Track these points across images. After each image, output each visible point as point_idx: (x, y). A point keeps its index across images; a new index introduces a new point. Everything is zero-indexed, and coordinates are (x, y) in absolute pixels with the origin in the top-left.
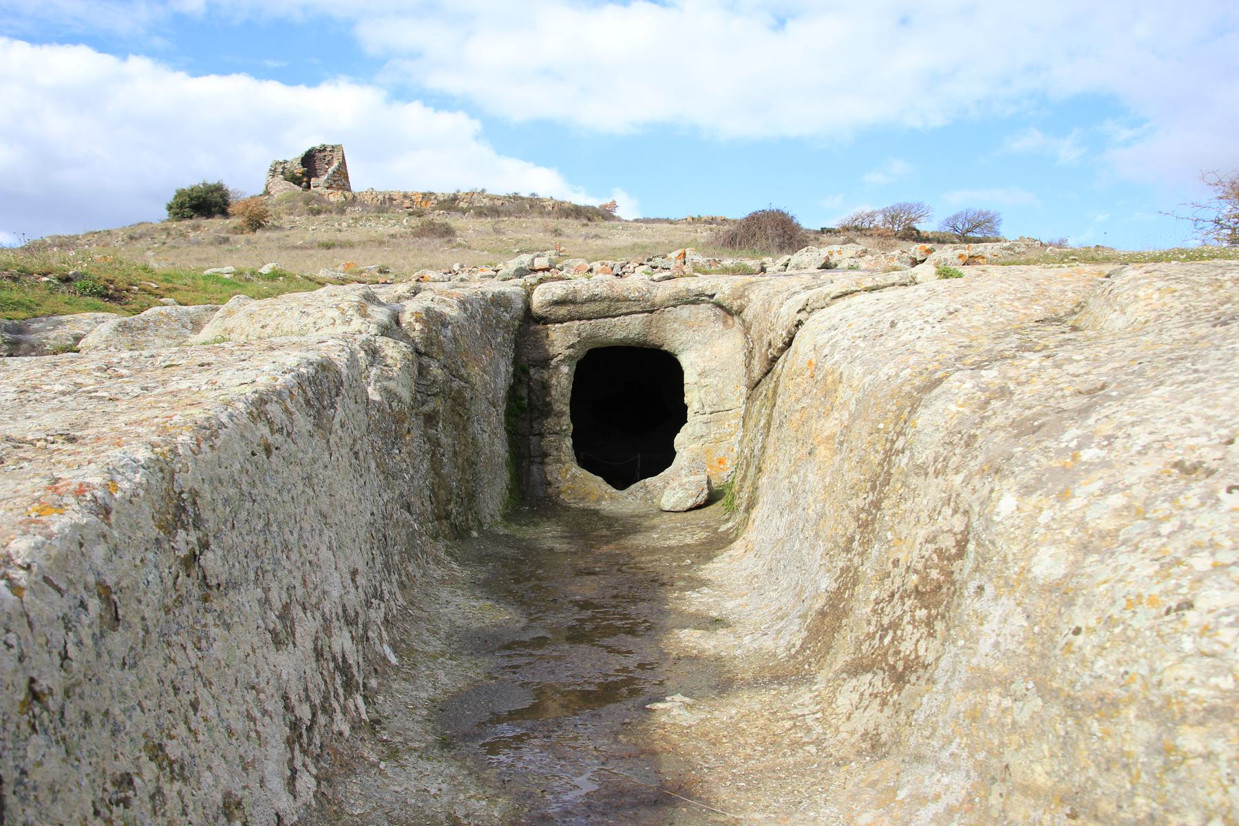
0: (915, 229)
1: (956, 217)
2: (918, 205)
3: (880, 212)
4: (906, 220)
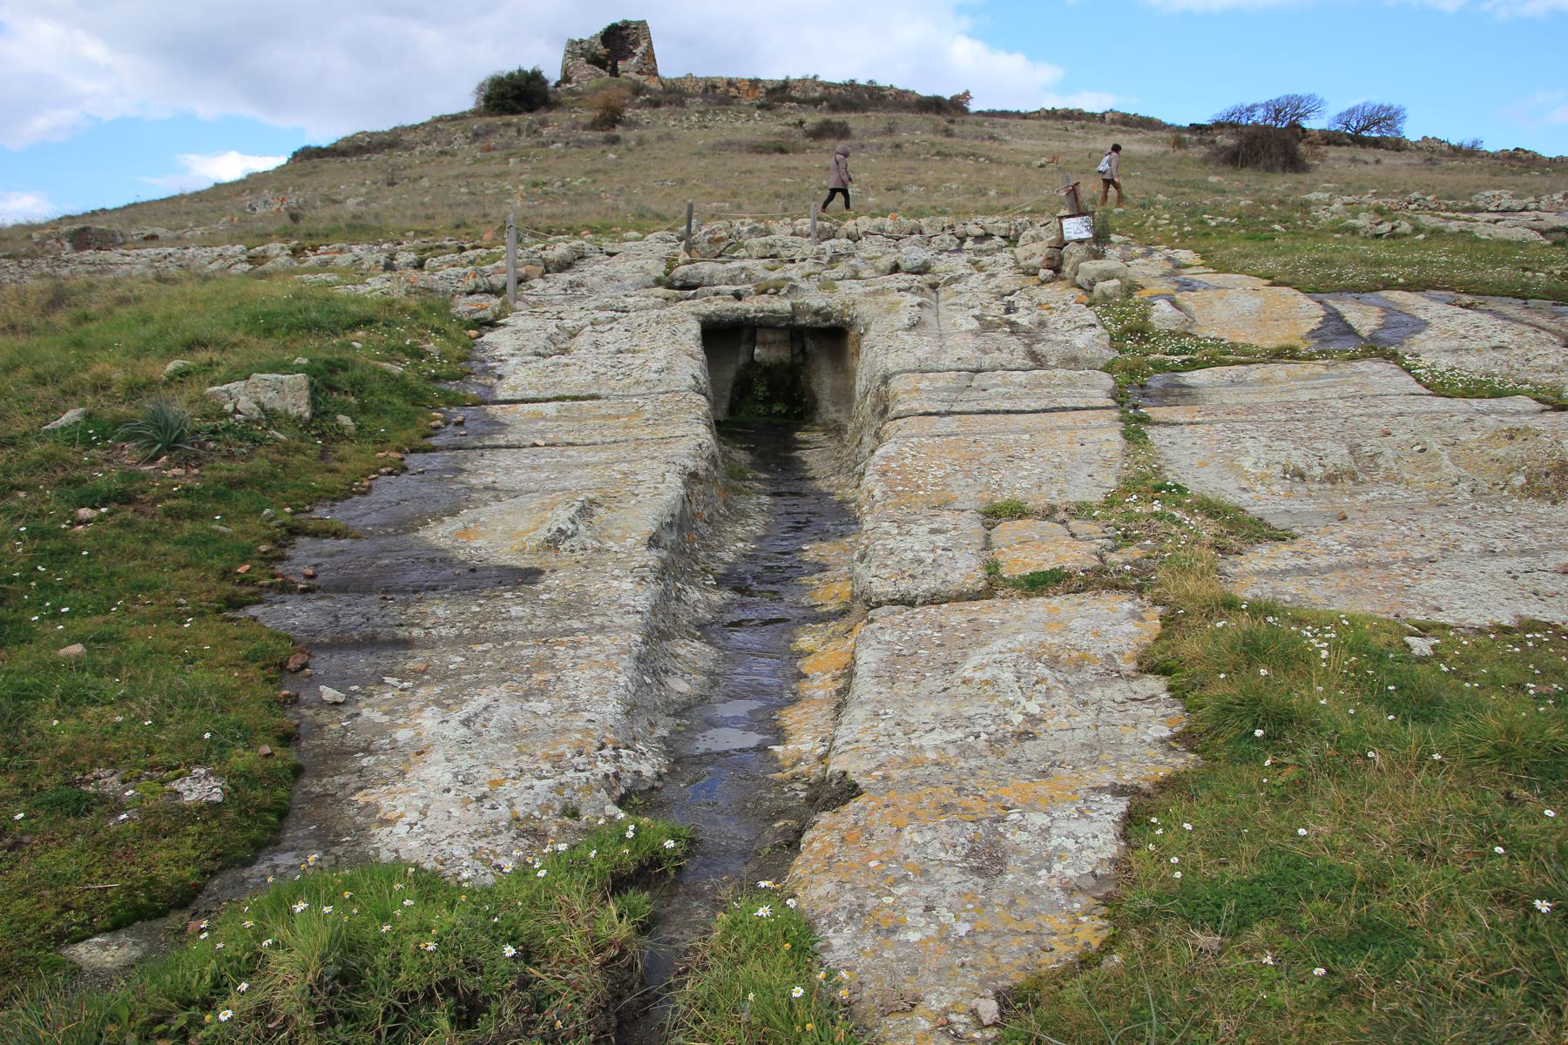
0: (1299, 126)
1: (1351, 112)
2: (1309, 98)
3: (1263, 106)
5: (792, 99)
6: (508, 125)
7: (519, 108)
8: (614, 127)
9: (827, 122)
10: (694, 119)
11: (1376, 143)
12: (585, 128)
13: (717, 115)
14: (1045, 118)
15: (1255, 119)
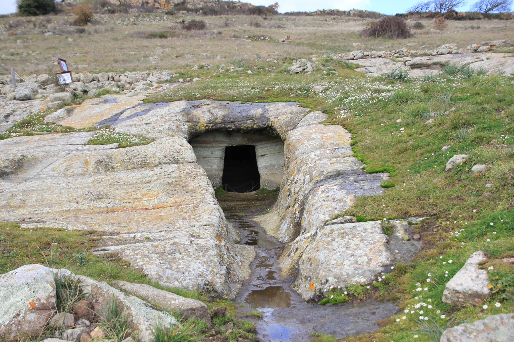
0: (454, 11)
3: (433, 2)
4: (449, 6)
5: (185, 9)
6: (30, 22)
7: (38, 12)
8: (86, 24)
9: (194, 21)
10: (132, 20)
11: (498, 17)
12: (71, 24)
13: (144, 17)
14: (319, 15)
15: (430, 9)
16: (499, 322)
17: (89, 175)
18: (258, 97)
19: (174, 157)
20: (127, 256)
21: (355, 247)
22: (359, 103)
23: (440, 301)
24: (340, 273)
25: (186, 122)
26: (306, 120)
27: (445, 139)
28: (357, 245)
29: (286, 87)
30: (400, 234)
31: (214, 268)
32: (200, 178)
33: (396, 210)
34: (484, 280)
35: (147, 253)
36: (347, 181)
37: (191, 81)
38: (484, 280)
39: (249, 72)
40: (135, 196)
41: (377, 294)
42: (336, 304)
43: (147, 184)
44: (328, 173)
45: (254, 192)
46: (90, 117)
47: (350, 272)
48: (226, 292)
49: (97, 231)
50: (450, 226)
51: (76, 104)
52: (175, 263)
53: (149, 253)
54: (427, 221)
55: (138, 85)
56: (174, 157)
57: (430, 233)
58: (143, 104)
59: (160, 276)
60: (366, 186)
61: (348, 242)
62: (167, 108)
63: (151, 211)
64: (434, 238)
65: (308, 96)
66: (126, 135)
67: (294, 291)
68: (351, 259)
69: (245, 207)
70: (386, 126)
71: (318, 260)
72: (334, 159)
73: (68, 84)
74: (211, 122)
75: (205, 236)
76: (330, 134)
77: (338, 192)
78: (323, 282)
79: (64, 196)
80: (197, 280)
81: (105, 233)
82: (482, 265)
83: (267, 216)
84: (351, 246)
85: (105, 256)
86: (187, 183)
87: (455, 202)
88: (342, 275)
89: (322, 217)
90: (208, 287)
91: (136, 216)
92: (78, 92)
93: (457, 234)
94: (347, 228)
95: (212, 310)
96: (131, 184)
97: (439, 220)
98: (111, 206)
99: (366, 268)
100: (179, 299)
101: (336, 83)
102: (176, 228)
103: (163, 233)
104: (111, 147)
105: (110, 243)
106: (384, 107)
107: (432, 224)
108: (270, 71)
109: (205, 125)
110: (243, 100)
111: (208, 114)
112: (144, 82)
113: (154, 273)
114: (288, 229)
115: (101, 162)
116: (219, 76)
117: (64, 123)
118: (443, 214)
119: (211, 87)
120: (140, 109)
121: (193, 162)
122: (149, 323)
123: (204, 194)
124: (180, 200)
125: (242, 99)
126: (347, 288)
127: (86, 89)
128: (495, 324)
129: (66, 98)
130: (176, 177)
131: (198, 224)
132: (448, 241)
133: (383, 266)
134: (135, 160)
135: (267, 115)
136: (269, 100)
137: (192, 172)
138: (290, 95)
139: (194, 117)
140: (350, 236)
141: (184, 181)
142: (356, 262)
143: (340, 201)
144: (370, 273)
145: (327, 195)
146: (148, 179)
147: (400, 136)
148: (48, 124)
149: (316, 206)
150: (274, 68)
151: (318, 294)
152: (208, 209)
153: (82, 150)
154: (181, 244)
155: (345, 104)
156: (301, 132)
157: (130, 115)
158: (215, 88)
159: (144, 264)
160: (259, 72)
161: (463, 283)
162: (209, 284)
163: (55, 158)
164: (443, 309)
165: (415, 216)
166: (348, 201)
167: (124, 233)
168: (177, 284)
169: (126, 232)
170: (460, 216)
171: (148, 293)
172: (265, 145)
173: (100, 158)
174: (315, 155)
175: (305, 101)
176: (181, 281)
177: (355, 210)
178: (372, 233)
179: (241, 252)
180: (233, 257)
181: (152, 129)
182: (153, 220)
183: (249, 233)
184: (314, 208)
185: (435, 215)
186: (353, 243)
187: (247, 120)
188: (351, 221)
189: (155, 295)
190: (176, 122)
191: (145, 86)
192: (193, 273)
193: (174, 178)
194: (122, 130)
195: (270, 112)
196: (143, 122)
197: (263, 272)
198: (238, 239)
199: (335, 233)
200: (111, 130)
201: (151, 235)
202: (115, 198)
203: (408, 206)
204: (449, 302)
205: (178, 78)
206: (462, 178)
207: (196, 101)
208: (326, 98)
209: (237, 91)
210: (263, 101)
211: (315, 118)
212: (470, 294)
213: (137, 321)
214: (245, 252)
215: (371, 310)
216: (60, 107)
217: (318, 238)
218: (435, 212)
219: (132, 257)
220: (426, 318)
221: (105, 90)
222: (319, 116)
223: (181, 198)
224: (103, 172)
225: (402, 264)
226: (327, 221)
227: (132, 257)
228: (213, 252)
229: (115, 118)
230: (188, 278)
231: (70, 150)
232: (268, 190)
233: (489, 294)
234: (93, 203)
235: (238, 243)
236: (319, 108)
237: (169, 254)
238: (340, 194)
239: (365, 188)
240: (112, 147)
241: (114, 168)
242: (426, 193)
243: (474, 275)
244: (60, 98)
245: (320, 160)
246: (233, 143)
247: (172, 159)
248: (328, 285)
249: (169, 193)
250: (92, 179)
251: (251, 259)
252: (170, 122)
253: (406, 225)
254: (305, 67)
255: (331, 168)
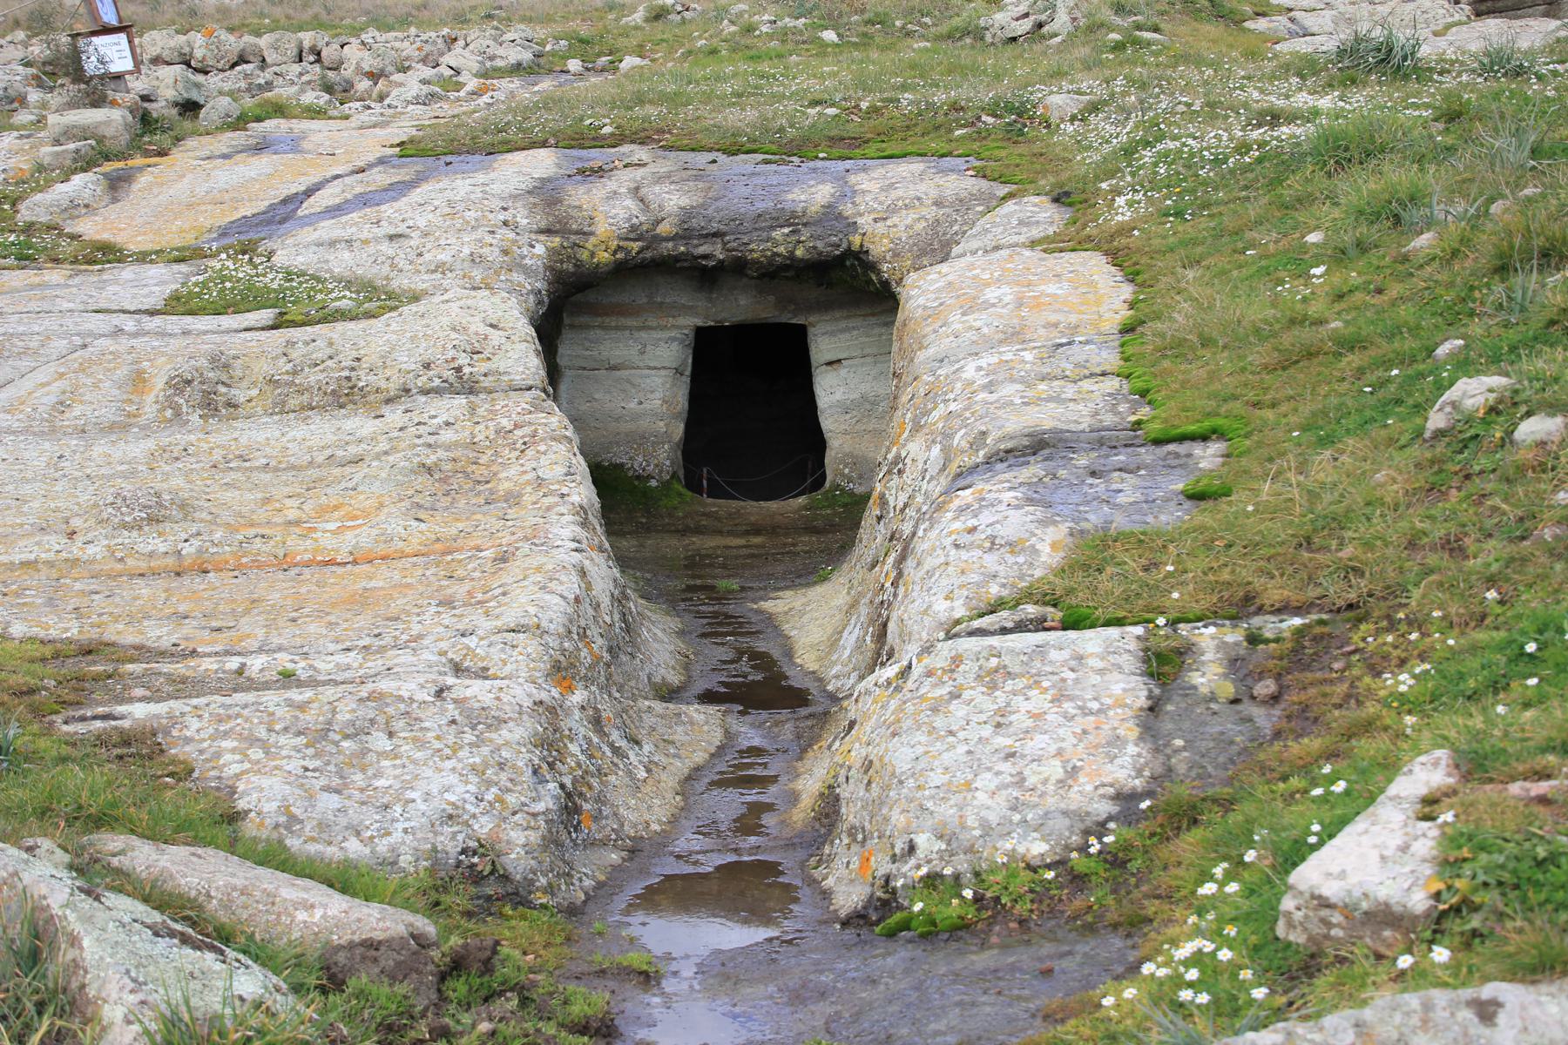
16: (1415, 1020)
17: (142, 428)
18: (831, 139)
19: (459, 369)
20: (188, 740)
21: (1029, 723)
22: (1188, 167)
23: (1270, 936)
24: (956, 820)
25: (541, 232)
26: (987, 231)
27: (1454, 317)
28: (1037, 716)
29: (940, 97)
30: (1208, 676)
31: (509, 790)
32: (542, 448)
33: (1213, 587)
34: (1424, 861)
35: (262, 733)
36: (1062, 473)
37: (612, 67)
38: (1424, 861)
39: (830, 36)
40: (292, 514)
41: (1078, 903)
42: (932, 934)
43: (348, 470)
44: (1003, 439)
45: (801, 500)
46: (190, 206)
47: (993, 818)
48: (543, 881)
49: (113, 644)
50: (1395, 653)
51: (147, 154)
52: (363, 770)
53: (270, 730)
54: (1318, 630)
55: (401, 85)
56: (459, 369)
57: (1319, 675)
58: (396, 161)
59: (293, 819)
60: (1128, 490)
61: (1008, 705)
62: (481, 177)
63: (340, 570)
64: (1325, 695)
65: (1021, 133)
66: (313, 277)
67: (813, 883)
68: (1006, 767)
69: (752, 556)
70: (1267, 257)
71: (890, 768)
72: (1042, 386)
73: (118, 77)
74: (635, 233)
75: (508, 669)
76: (1052, 288)
77: (1011, 512)
78: (897, 851)
79: (26, 507)
80: (436, 834)
81: (142, 652)
82: (1429, 806)
83: (819, 590)
84: (1013, 718)
85: (101, 740)
86: (495, 468)
87: (1432, 559)
88: (963, 827)
89: (941, 607)
90: (476, 860)
91: (276, 590)
92: (156, 109)
93: (1404, 682)
94: (1012, 651)
95: (445, 948)
96: (293, 467)
97: (1363, 627)
98: (192, 550)
99: (1051, 802)
100: (325, 906)
101: (1130, 80)
102: (405, 637)
103: (352, 658)
104: (245, 324)
105: (139, 692)
106: (1275, 182)
107: (1335, 643)
108: (908, 34)
109: (614, 244)
110: (774, 148)
111: (629, 203)
112: (428, 72)
113: (270, 807)
114: (861, 641)
115: (189, 382)
116: (714, 52)
117: (89, 228)
118: (1382, 604)
119: (663, 98)
120: (379, 177)
121: (529, 389)
122: (140, 996)
123: (548, 509)
124: (454, 531)
125: (768, 147)
126: (977, 874)
127: (194, 95)
128: (1398, 1028)
129: (109, 132)
130: (456, 444)
131: (485, 625)
132: (1371, 708)
133: (1118, 797)
134: (313, 377)
135: (848, 209)
136: (871, 150)
137: (516, 426)
138: (951, 131)
139: (574, 213)
140: (1020, 683)
141: (484, 459)
142: (1020, 780)
143: (1013, 546)
144: (1067, 822)
145: (972, 522)
146: (353, 450)
147: (1305, 300)
148: (29, 228)
149: (926, 567)
150: (927, 20)
151: (879, 894)
152: (539, 569)
153: (135, 335)
154: (400, 699)
155: (1140, 168)
156: (950, 278)
157: (337, 201)
158: (675, 100)
159: (243, 773)
160: (865, 35)
161: (1349, 869)
162: (483, 848)
163: (25, 363)
164: (1276, 963)
165: (1279, 611)
166: (1045, 548)
167: (209, 655)
168: (354, 848)
169: (218, 648)
170: (1437, 614)
171: (209, 881)
172: (843, 324)
173: (186, 369)
174: (980, 369)
175: (1003, 153)
176: (372, 838)
177: (1060, 585)
178: (1101, 672)
179: (661, 730)
180: (616, 750)
181: (412, 256)
182: (334, 605)
183: (730, 655)
184: (921, 573)
185: (1350, 606)
186: (1024, 706)
187: (772, 228)
188: (1040, 625)
189: (234, 889)
190: (504, 231)
191: (426, 89)
192: (423, 807)
193: (448, 448)
194: (300, 259)
195: (858, 200)
196: (380, 232)
197: (730, 804)
198: (675, 679)
199: (969, 668)
200: (257, 260)
201: (302, 664)
202: (214, 521)
203: (1261, 571)
204: (1298, 937)
205: (565, 58)
206: (1477, 468)
207: (594, 152)
208: (1081, 145)
209: (751, 114)
210: (846, 152)
211: (1021, 223)
212: (1366, 913)
213: (99, 991)
214: (680, 729)
215: (1040, 959)
216: (85, 164)
217: (910, 684)
218: (1352, 596)
219: (205, 745)
220: (1203, 998)
221: (268, 102)
222: (1041, 214)
223: (460, 526)
224: (195, 418)
225: (1184, 791)
226: (958, 622)
227: (205, 745)
228: (516, 733)
229: (284, 213)
230: (400, 826)
231: (91, 334)
232: (852, 494)
233: (1427, 914)
234: (126, 537)
235: (668, 694)
236: (1042, 182)
237: (347, 737)
238: (1015, 522)
239: (1121, 499)
240: (252, 324)
241: (236, 406)
242: (1337, 523)
243: (1396, 840)
244: (84, 129)
245: (990, 387)
246: (724, 315)
247: (449, 375)
248: (913, 862)
249: (419, 506)
250: (150, 444)
251: (700, 757)
252: (479, 234)
253: (1237, 644)
254: (1043, 17)
255: (1016, 423)
